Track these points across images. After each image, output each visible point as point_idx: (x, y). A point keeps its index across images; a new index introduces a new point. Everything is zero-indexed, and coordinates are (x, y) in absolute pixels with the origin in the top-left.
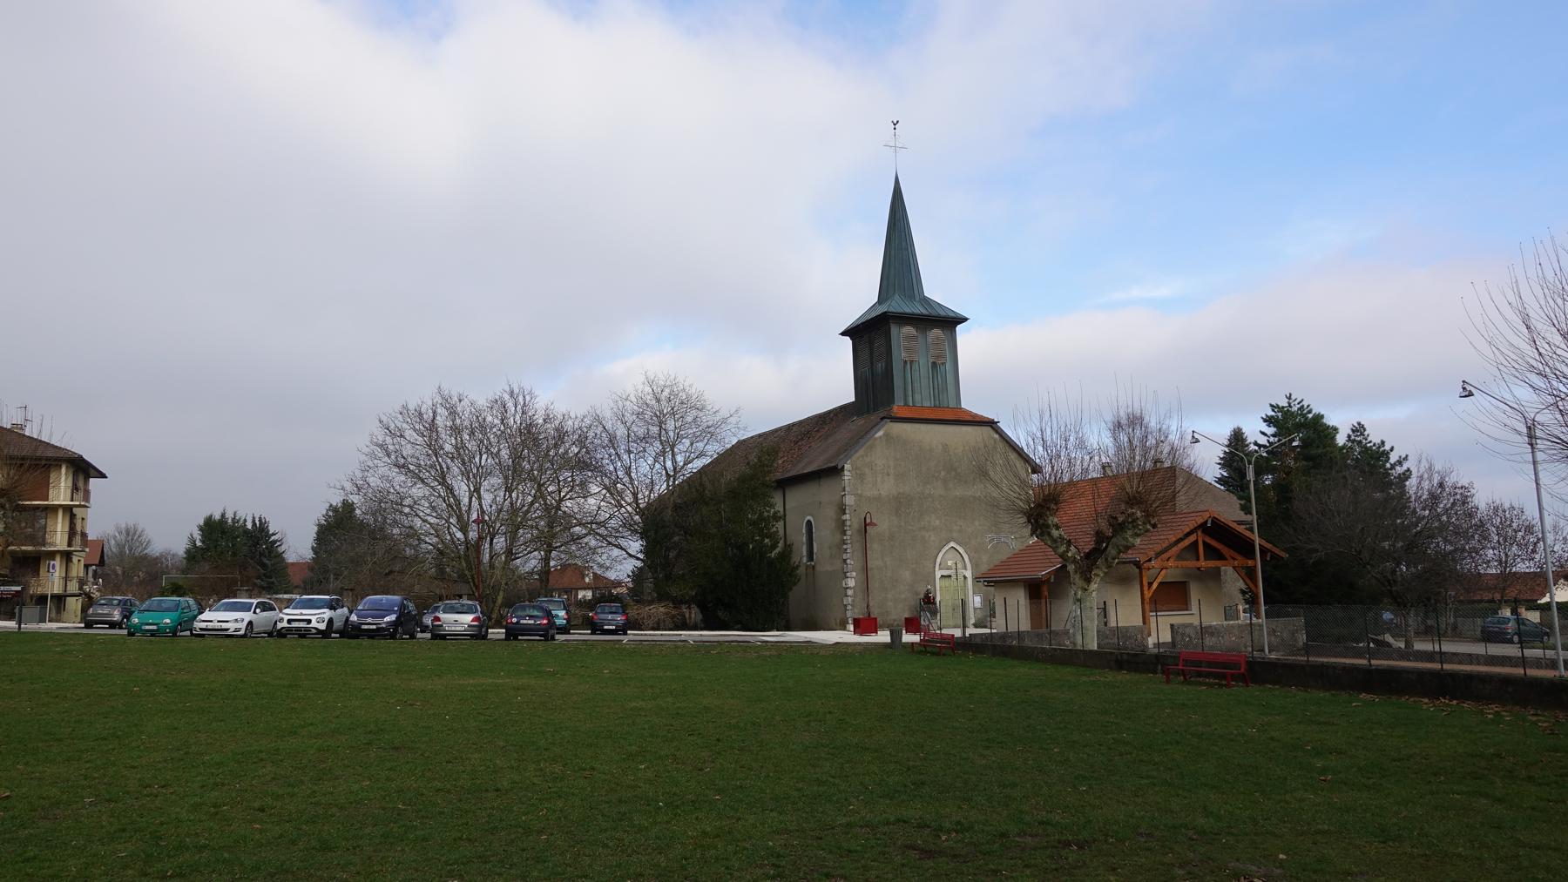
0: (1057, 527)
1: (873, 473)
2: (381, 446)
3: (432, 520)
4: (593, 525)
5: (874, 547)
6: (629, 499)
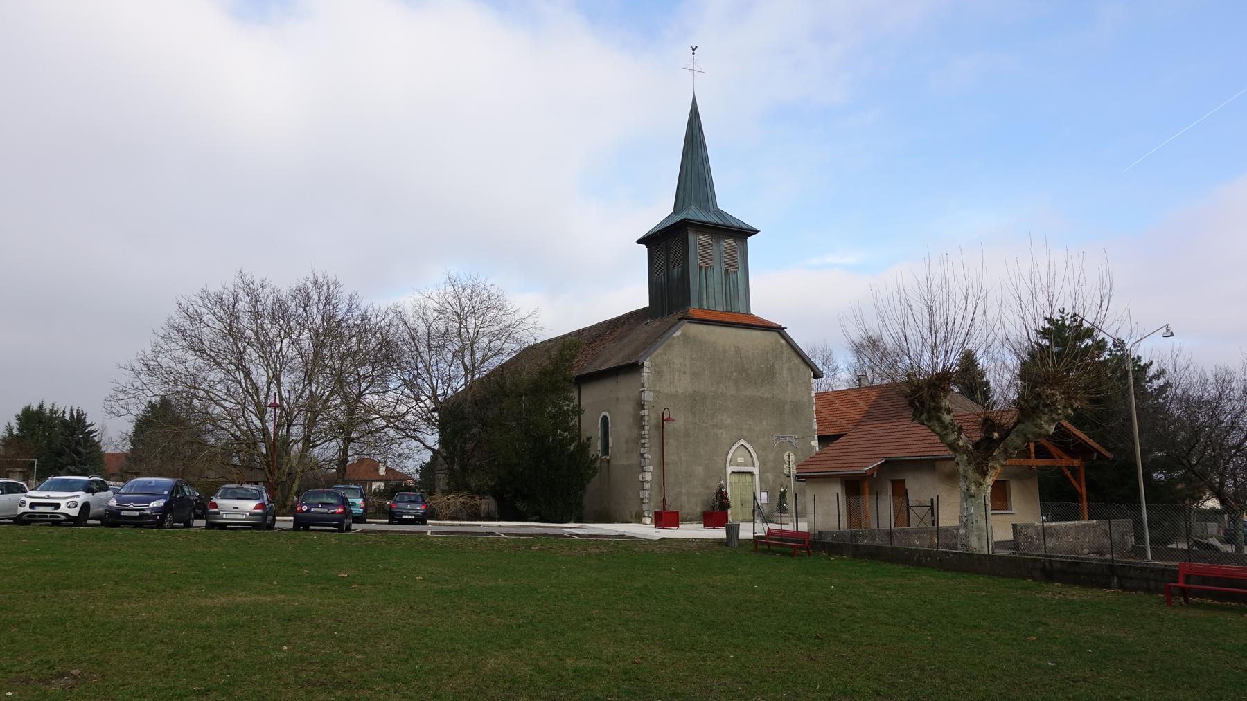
0: (949, 412)
1: (671, 371)
2: (178, 330)
3: (227, 404)
4: (394, 419)
5: (671, 442)
6: (428, 392)
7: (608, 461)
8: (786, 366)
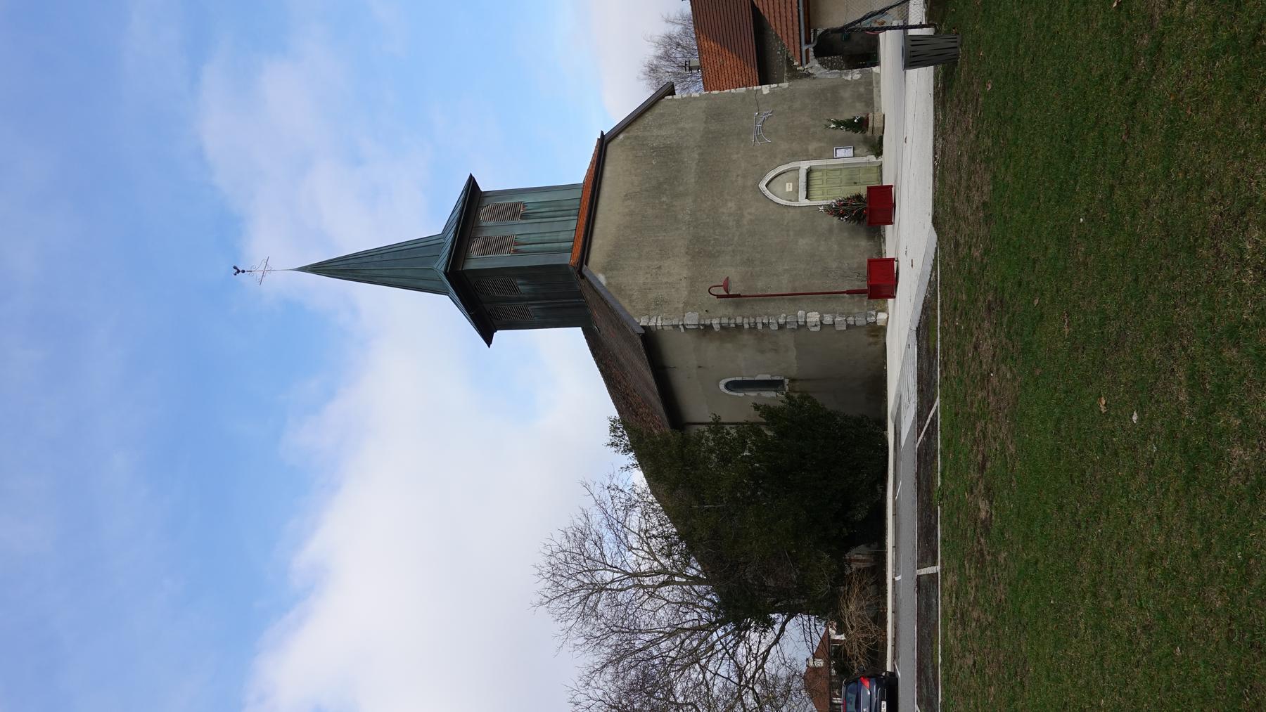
1: (656, 286)
5: (761, 285)
7: (792, 380)
8: (656, 132)
